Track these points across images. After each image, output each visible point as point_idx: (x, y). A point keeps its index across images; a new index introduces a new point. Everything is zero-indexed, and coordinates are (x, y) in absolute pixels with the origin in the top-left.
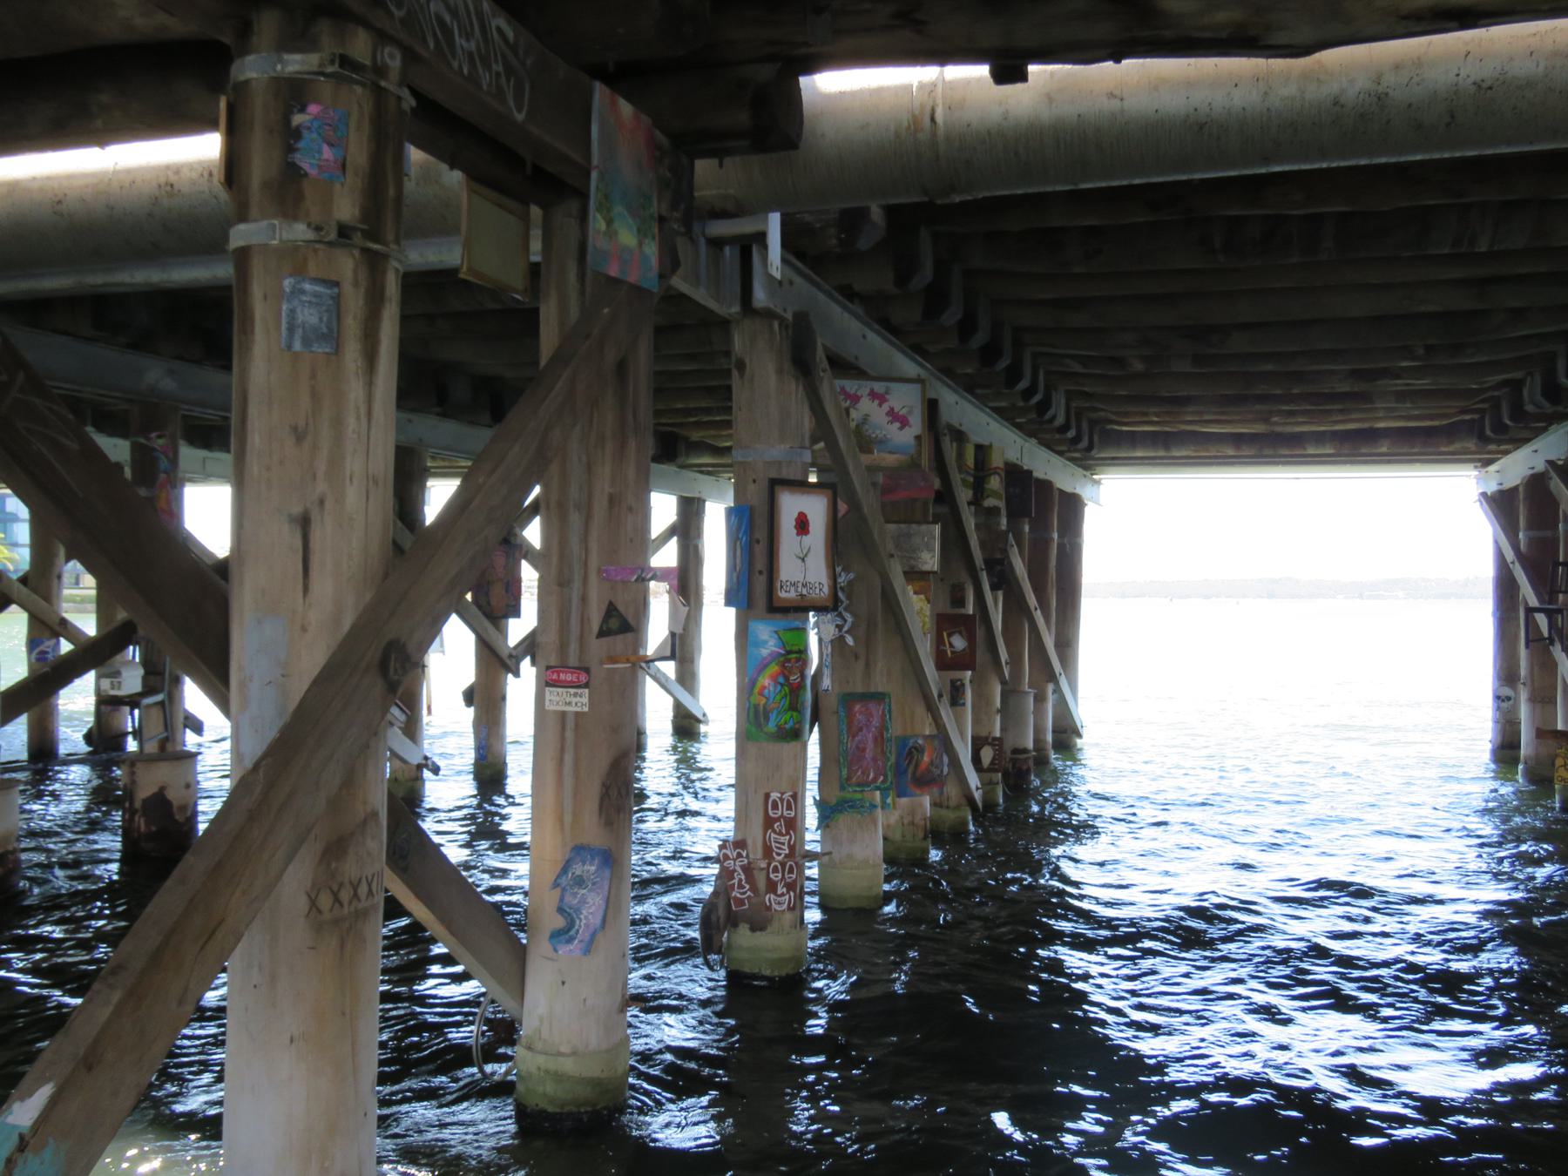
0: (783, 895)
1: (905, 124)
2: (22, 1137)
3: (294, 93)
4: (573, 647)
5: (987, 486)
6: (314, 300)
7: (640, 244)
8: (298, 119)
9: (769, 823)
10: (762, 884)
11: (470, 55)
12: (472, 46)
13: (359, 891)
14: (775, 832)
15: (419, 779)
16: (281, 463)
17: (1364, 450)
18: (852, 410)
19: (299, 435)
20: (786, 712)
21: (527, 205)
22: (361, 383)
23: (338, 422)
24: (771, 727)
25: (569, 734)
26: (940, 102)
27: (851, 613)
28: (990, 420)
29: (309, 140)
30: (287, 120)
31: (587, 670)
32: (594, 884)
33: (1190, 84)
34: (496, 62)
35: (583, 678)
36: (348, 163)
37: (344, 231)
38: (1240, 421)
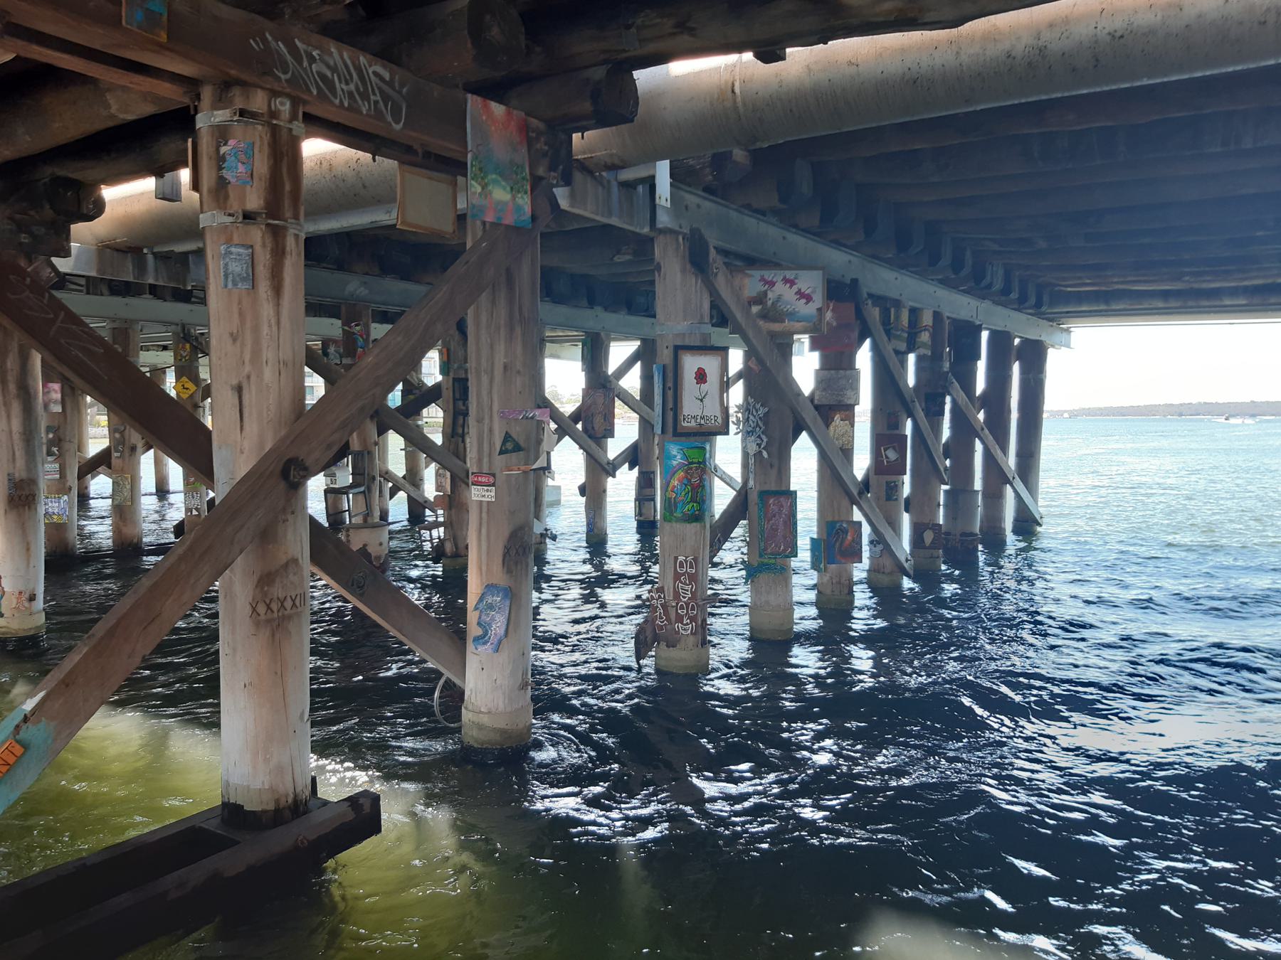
0: (687, 624)
1: (716, 96)
2: (25, 715)
3: (222, 133)
4: (486, 460)
5: (918, 340)
6: (238, 257)
7: (514, 198)
8: (223, 149)
9: (677, 576)
10: (673, 616)
11: (350, 94)
12: (352, 87)
13: (285, 604)
14: (682, 583)
15: (543, 543)
16: (226, 355)
17: (1273, 300)
18: (769, 292)
19: (234, 338)
20: (689, 503)
21: (456, 177)
22: (271, 305)
23: (256, 330)
24: (678, 514)
25: (484, 515)
26: (737, 78)
27: (766, 436)
28: (936, 289)
29: (230, 161)
30: (218, 150)
31: (494, 475)
32: (499, 609)
33: (903, 50)
34: (374, 94)
35: (492, 480)
36: (255, 173)
37: (248, 216)
38: (1146, 282)
